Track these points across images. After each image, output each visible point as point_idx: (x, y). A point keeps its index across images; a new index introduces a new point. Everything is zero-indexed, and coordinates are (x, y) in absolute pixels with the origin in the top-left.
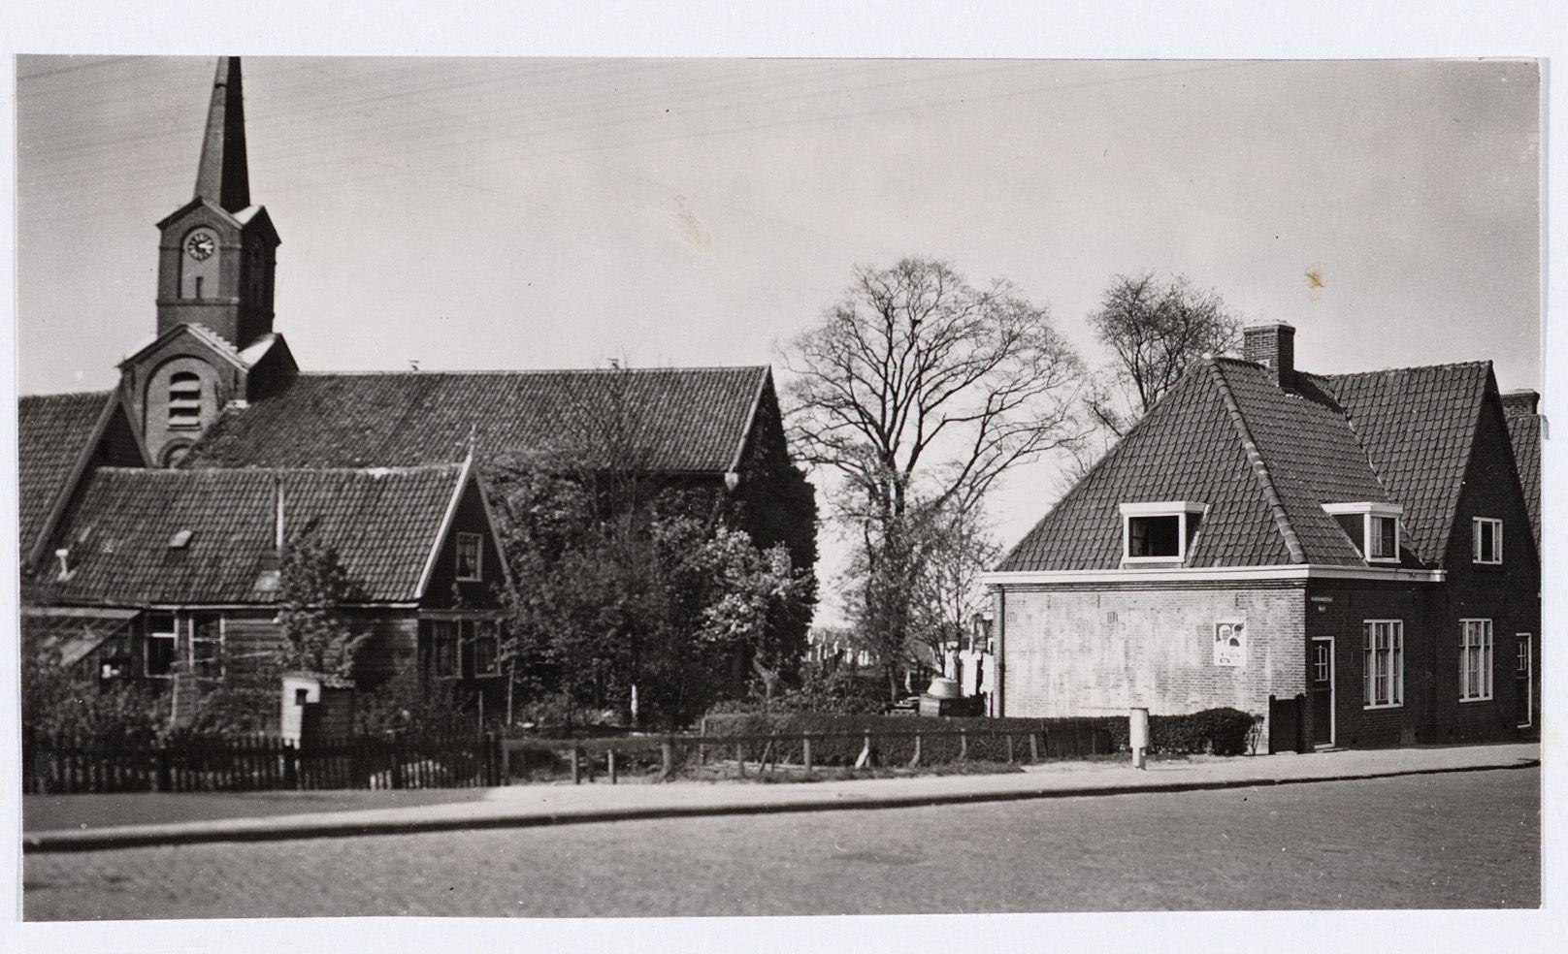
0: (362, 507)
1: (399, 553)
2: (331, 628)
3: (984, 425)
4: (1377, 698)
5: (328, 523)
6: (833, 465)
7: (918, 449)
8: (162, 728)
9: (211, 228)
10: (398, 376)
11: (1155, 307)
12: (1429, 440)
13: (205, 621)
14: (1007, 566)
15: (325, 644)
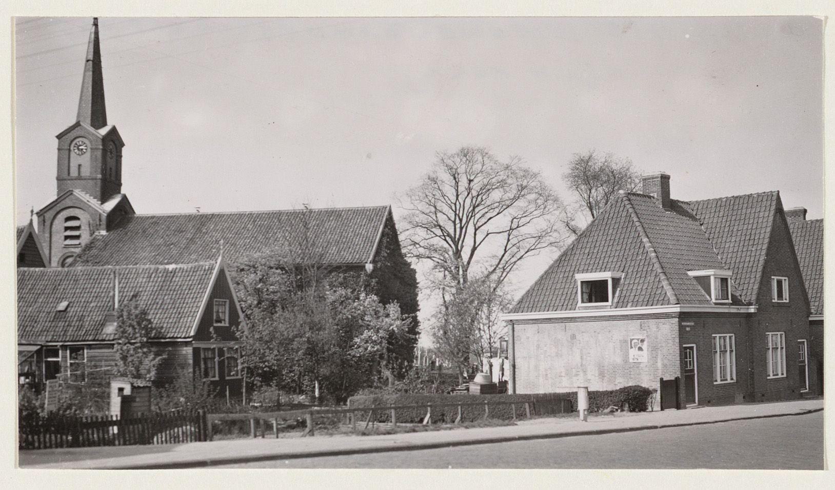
0: (162, 286)
1: (182, 311)
2: (144, 353)
3: (509, 235)
4: (721, 377)
5: (143, 295)
6: (429, 260)
7: (474, 249)
8: (42, 411)
9: (85, 138)
10: (189, 215)
11: (597, 170)
12: (746, 235)
13: (76, 350)
14: (516, 310)
15: (141, 363)
